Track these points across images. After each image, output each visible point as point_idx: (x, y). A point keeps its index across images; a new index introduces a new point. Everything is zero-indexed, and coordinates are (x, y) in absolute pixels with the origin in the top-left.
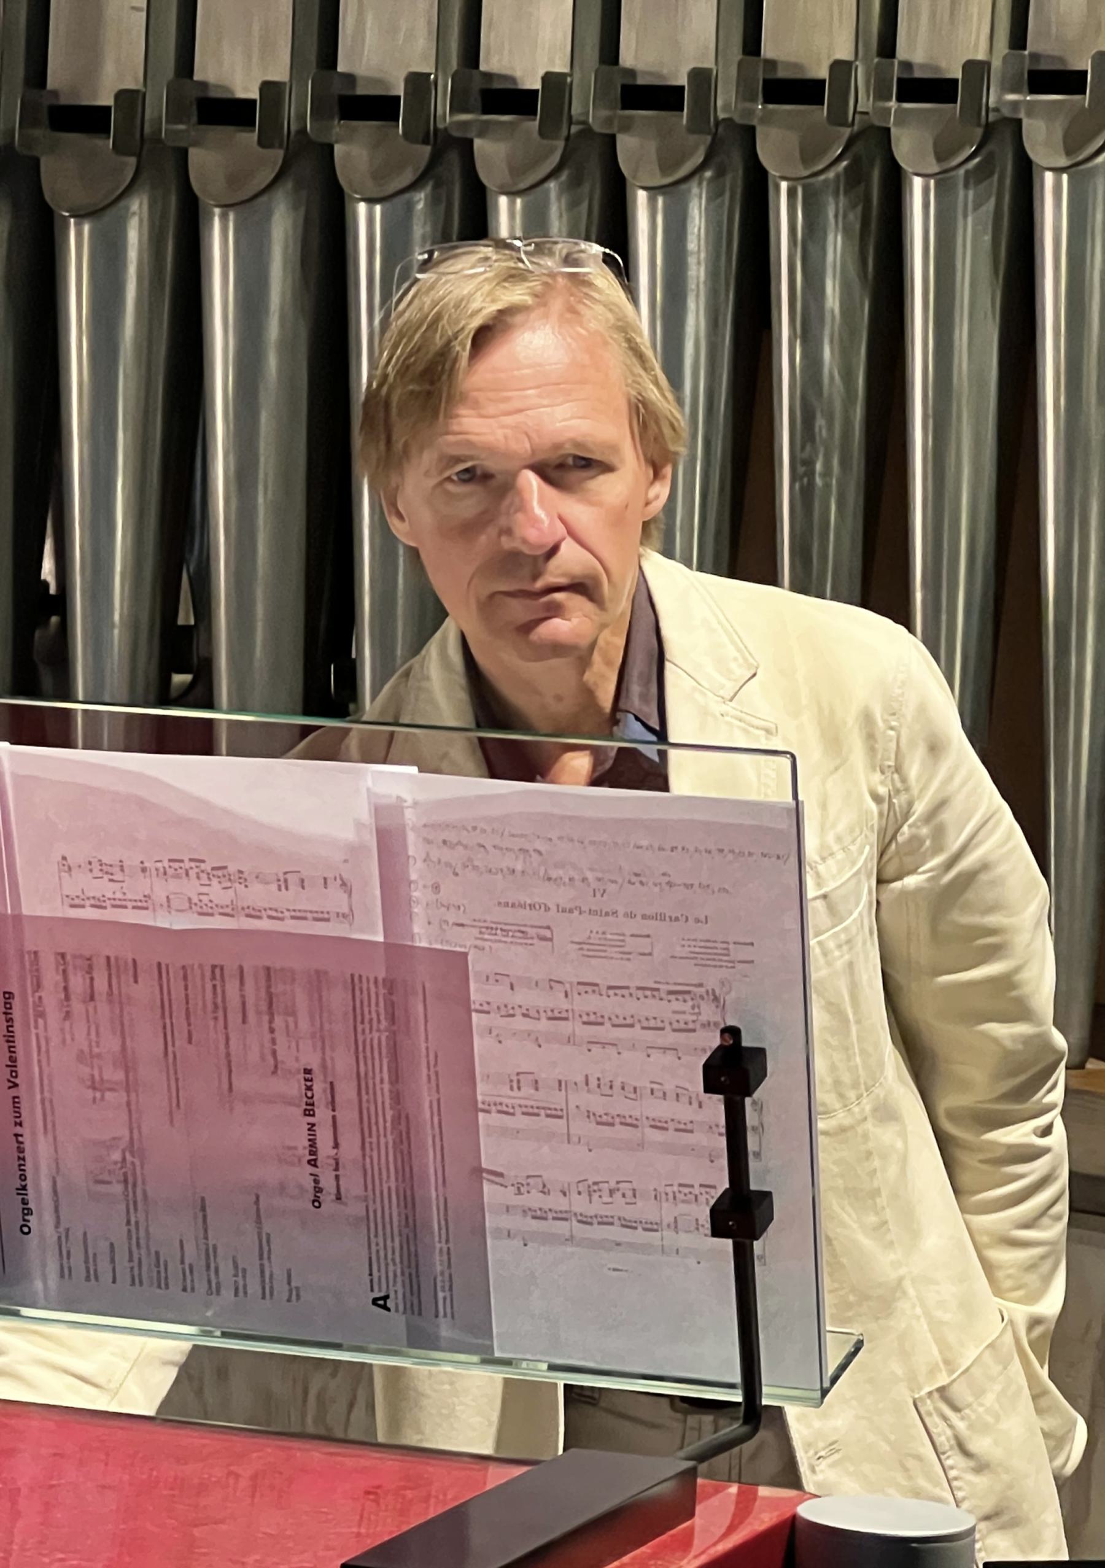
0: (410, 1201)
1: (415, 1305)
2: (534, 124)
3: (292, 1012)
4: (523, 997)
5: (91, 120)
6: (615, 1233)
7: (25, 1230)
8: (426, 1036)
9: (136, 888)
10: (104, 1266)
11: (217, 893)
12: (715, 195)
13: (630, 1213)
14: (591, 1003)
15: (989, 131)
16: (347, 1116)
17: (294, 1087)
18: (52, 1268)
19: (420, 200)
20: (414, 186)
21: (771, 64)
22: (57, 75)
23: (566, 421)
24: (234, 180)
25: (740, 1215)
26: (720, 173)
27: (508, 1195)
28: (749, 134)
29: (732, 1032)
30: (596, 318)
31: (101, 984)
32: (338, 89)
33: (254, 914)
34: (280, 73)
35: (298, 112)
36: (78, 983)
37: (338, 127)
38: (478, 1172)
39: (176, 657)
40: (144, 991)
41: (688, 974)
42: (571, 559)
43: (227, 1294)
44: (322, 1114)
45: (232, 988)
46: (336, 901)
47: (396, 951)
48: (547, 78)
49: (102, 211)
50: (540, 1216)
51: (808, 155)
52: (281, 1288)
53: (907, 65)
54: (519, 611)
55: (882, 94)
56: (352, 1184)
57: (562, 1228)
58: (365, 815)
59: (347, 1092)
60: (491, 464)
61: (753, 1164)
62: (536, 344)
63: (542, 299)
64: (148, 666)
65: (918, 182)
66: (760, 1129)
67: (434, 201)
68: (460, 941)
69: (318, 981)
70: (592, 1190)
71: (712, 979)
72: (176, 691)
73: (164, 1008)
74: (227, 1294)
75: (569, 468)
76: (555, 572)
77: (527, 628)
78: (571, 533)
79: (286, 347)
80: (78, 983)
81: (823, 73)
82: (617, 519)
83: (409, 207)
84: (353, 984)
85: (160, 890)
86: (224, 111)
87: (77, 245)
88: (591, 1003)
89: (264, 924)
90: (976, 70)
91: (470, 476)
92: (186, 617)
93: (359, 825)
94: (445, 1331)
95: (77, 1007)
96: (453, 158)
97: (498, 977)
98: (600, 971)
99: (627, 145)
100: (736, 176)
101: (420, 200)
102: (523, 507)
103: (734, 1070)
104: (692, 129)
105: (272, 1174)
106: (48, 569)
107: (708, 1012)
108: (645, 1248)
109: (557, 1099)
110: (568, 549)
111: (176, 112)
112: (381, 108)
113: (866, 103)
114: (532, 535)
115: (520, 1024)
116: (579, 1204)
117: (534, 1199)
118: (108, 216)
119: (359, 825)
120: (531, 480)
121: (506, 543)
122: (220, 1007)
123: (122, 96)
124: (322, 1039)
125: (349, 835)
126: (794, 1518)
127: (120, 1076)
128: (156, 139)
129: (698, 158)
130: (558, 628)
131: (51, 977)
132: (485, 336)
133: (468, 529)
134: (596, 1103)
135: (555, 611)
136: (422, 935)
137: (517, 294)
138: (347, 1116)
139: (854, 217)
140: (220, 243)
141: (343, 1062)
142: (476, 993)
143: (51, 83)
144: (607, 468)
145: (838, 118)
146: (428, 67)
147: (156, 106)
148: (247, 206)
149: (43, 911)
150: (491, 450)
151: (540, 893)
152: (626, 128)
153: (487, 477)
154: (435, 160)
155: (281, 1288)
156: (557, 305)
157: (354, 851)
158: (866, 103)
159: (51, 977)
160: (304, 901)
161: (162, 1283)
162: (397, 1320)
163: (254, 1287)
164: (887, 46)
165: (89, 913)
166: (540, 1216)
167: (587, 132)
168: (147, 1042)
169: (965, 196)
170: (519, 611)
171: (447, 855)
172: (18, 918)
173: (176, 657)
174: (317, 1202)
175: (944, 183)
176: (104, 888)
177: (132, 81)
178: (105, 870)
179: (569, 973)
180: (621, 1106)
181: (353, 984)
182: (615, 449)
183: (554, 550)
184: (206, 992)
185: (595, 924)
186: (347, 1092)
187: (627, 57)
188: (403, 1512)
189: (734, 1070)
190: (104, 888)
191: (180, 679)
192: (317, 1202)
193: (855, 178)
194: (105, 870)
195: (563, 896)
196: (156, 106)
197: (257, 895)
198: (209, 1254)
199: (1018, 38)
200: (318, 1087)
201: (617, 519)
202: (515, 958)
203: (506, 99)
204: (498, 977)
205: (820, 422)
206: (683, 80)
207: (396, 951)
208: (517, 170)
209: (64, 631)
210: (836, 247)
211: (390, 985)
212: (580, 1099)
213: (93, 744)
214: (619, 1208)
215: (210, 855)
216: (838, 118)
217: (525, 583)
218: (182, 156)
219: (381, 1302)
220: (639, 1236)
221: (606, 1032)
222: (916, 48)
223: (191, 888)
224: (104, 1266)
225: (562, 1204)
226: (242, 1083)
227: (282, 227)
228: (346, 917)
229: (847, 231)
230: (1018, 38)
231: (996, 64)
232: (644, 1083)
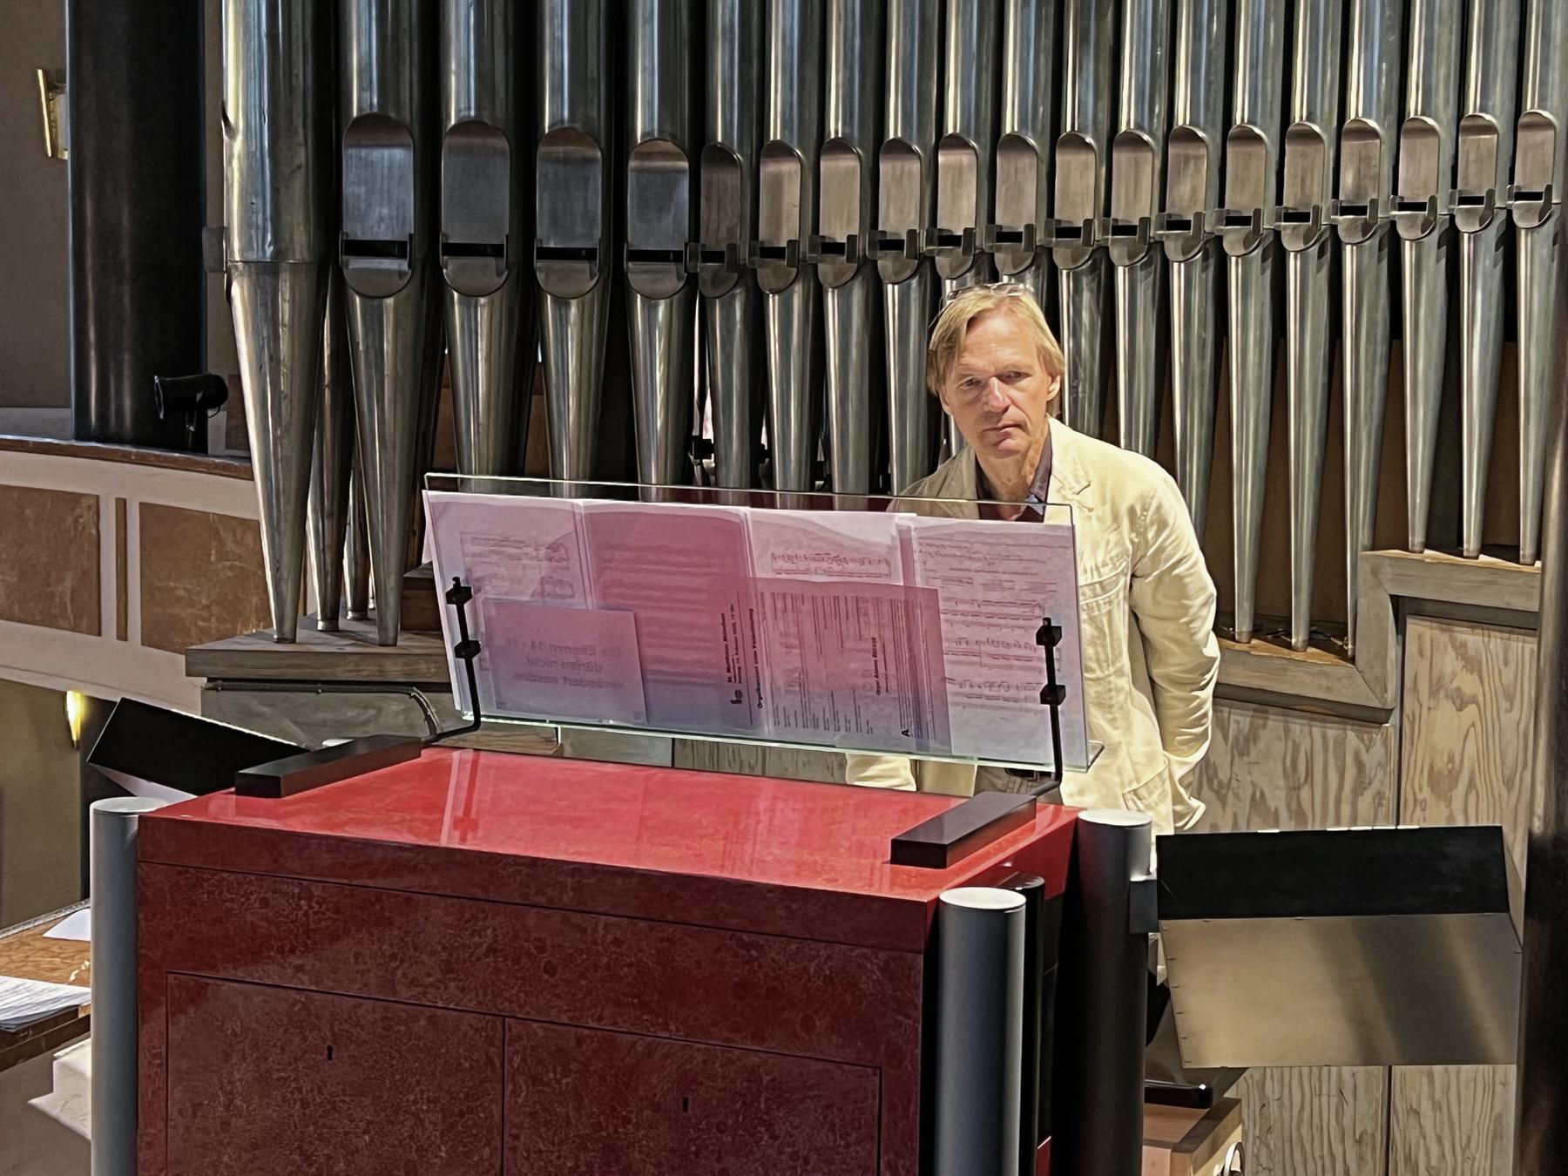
0: (916, 690)
1: (919, 735)
2: (960, 250)
3: (866, 614)
4: (961, 607)
5: (777, 253)
6: (1001, 703)
7: (760, 705)
8: (922, 623)
9: (802, 565)
10: (792, 719)
11: (835, 567)
12: (1036, 276)
13: (1007, 694)
14: (991, 609)
15: (1150, 245)
16: (891, 657)
17: (869, 645)
18: (771, 722)
19: (914, 282)
20: (912, 276)
21: (1059, 222)
22: (763, 233)
23: (1009, 356)
24: (837, 276)
25: (1053, 695)
26: (1038, 268)
27: (956, 688)
28: (1050, 251)
29: (1048, 620)
30: (1022, 314)
31: (790, 606)
32: (878, 238)
33: (851, 575)
34: (855, 231)
35: (862, 246)
36: (780, 605)
37: (879, 253)
38: (944, 679)
39: (817, 469)
40: (807, 607)
41: (1028, 596)
42: (1014, 414)
43: (843, 731)
44: (880, 656)
45: (842, 604)
46: (883, 568)
47: (909, 589)
48: (966, 230)
49: (784, 291)
50: (970, 696)
51: (1075, 259)
52: (864, 728)
53: (1116, 220)
54: (992, 437)
55: (1105, 232)
56: (893, 684)
57: (979, 701)
58: (894, 532)
59: (890, 647)
60: (979, 377)
61: (1057, 674)
62: (997, 325)
63: (998, 306)
64: (805, 479)
65: (1120, 269)
66: (1059, 660)
67: (920, 283)
68: (937, 584)
69: (877, 602)
70: (991, 685)
71: (1039, 598)
72: (817, 488)
73: (815, 615)
74: (843, 731)
75: (1011, 376)
76: (1007, 419)
77: (997, 444)
78: (1014, 403)
79: (860, 345)
80: (780, 605)
81: (1081, 224)
82: (1034, 397)
83: (909, 286)
84: (892, 602)
85: (813, 565)
86: (833, 248)
87: (773, 304)
88: (991, 609)
89: (855, 579)
90: (1145, 221)
91: (971, 383)
92: (821, 457)
93: (893, 538)
94: (932, 743)
95: (780, 614)
96: (928, 264)
97: (949, 599)
98: (995, 596)
99: (998, 257)
100: (1044, 269)
101: (914, 282)
102: (992, 392)
103: (1048, 636)
104: (1027, 249)
105: (859, 681)
106: (764, 440)
107: (1037, 612)
108: (1012, 709)
109: (976, 648)
110: (1012, 409)
111: (812, 249)
112: (896, 245)
113: (1098, 236)
114: (995, 403)
115: (959, 618)
116: (986, 691)
117: (967, 689)
118: (786, 293)
119: (893, 538)
120: (995, 381)
121: (986, 408)
122: (837, 614)
123: (790, 242)
124: (880, 626)
125: (888, 541)
126: (1077, 820)
127: (796, 642)
128: (804, 260)
129: (1028, 262)
130: (1009, 443)
131: (768, 602)
132: (972, 323)
133: (972, 403)
134: (991, 649)
135: (1008, 435)
136: (919, 582)
137: (988, 304)
138: (891, 657)
139: (1094, 285)
140: (832, 302)
141: (888, 634)
142: (942, 605)
143: (761, 238)
144: (1028, 375)
145: (1087, 243)
146: (916, 227)
147: (804, 246)
148: (843, 288)
149: (764, 575)
150: (979, 371)
151: (967, 564)
152: (999, 249)
153: (978, 382)
154: (919, 265)
155: (864, 728)
156: (1004, 308)
157: (891, 548)
158: (1098, 236)
159: (768, 602)
160: (872, 569)
161: (816, 726)
162: (912, 741)
163: (854, 727)
164: (1107, 212)
165: (783, 576)
166: (970, 696)
167: (983, 252)
168: (808, 628)
169: (1140, 274)
170: (992, 437)
171: (928, 549)
172: (755, 579)
173: (817, 469)
174: (878, 692)
175: (1131, 269)
176: (789, 566)
177: (795, 236)
178: (790, 558)
179: (980, 597)
180: (1003, 651)
181: (892, 602)
182: (1031, 367)
183: (1006, 409)
184: (833, 606)
185: (990, 577)
186: (890, 647)
187: (999, 220)
188: (917, 819)
189: (1048, 636)
190: (789, 566)
191: (819, 483)
192: (878, 692)
193: (1094, 269)
194: (790, 558)
195: (977, 565)
196: (804, 246)
197: (851, 567)
198: (835, 714)
199: (1162, 208)
200: (878, 645)
201: (1034, 397)
202: (957, 590)
203: (949, 240)
204: (949, 599)
205: (1081, 370)
206: (1022, 229)
207: (909, 589)
208: (953, 270)
209: (771, 464)
210: (1086, 296)
211: (906, 602)
212: (984, 648)
213: (784, 507)
214: (1002, 692)
215: (835, 551)
216: (1087, 243)
217: (994, 425)
218: (815, 266)
219: (905, 733)
220: (1011, 704)
221: (995, 621)
222: (1118, 213)
223: (825, 565)
224: (792, 719)
225: (978, 691)
226: (848, 644)
227: (857, 295)
228: (889, 575)
229: (1091, 291)
230: (1162, 208)
231: (1153, 219)
232: (1012, 641)
